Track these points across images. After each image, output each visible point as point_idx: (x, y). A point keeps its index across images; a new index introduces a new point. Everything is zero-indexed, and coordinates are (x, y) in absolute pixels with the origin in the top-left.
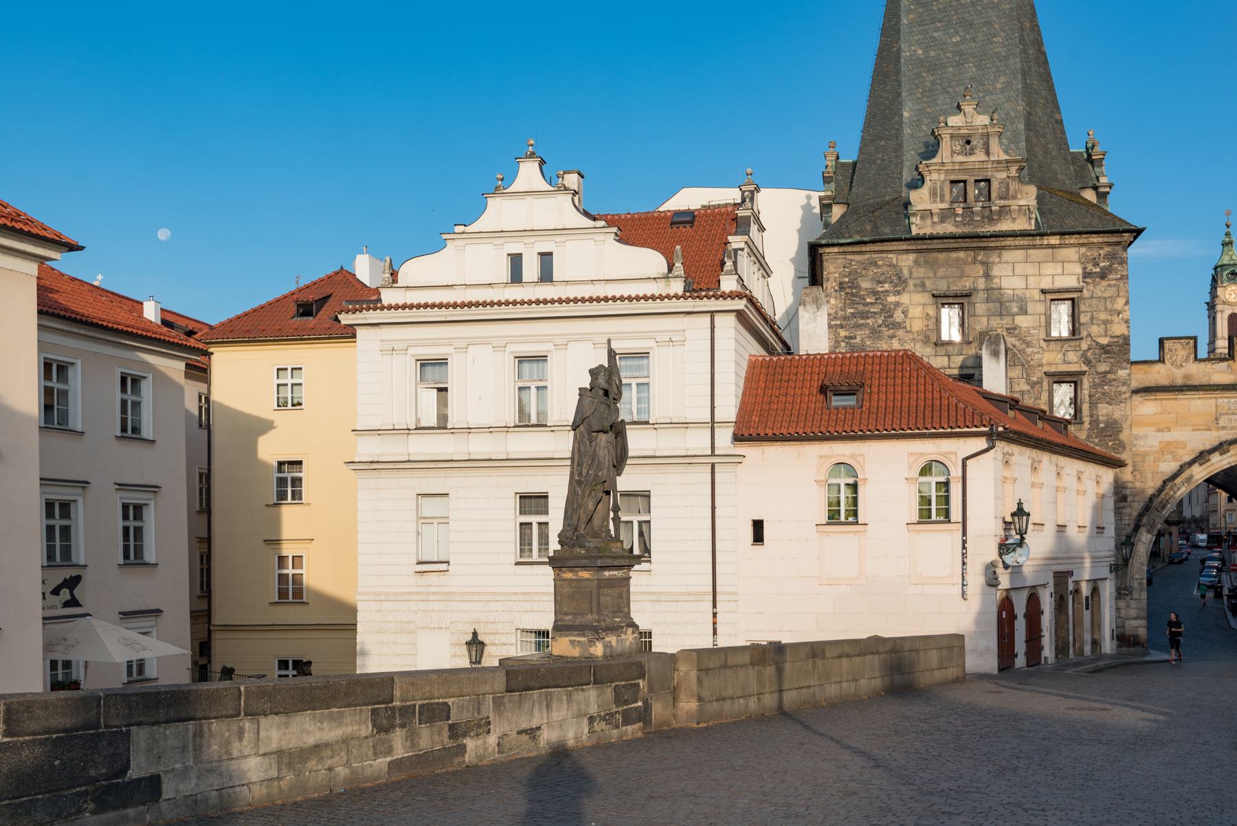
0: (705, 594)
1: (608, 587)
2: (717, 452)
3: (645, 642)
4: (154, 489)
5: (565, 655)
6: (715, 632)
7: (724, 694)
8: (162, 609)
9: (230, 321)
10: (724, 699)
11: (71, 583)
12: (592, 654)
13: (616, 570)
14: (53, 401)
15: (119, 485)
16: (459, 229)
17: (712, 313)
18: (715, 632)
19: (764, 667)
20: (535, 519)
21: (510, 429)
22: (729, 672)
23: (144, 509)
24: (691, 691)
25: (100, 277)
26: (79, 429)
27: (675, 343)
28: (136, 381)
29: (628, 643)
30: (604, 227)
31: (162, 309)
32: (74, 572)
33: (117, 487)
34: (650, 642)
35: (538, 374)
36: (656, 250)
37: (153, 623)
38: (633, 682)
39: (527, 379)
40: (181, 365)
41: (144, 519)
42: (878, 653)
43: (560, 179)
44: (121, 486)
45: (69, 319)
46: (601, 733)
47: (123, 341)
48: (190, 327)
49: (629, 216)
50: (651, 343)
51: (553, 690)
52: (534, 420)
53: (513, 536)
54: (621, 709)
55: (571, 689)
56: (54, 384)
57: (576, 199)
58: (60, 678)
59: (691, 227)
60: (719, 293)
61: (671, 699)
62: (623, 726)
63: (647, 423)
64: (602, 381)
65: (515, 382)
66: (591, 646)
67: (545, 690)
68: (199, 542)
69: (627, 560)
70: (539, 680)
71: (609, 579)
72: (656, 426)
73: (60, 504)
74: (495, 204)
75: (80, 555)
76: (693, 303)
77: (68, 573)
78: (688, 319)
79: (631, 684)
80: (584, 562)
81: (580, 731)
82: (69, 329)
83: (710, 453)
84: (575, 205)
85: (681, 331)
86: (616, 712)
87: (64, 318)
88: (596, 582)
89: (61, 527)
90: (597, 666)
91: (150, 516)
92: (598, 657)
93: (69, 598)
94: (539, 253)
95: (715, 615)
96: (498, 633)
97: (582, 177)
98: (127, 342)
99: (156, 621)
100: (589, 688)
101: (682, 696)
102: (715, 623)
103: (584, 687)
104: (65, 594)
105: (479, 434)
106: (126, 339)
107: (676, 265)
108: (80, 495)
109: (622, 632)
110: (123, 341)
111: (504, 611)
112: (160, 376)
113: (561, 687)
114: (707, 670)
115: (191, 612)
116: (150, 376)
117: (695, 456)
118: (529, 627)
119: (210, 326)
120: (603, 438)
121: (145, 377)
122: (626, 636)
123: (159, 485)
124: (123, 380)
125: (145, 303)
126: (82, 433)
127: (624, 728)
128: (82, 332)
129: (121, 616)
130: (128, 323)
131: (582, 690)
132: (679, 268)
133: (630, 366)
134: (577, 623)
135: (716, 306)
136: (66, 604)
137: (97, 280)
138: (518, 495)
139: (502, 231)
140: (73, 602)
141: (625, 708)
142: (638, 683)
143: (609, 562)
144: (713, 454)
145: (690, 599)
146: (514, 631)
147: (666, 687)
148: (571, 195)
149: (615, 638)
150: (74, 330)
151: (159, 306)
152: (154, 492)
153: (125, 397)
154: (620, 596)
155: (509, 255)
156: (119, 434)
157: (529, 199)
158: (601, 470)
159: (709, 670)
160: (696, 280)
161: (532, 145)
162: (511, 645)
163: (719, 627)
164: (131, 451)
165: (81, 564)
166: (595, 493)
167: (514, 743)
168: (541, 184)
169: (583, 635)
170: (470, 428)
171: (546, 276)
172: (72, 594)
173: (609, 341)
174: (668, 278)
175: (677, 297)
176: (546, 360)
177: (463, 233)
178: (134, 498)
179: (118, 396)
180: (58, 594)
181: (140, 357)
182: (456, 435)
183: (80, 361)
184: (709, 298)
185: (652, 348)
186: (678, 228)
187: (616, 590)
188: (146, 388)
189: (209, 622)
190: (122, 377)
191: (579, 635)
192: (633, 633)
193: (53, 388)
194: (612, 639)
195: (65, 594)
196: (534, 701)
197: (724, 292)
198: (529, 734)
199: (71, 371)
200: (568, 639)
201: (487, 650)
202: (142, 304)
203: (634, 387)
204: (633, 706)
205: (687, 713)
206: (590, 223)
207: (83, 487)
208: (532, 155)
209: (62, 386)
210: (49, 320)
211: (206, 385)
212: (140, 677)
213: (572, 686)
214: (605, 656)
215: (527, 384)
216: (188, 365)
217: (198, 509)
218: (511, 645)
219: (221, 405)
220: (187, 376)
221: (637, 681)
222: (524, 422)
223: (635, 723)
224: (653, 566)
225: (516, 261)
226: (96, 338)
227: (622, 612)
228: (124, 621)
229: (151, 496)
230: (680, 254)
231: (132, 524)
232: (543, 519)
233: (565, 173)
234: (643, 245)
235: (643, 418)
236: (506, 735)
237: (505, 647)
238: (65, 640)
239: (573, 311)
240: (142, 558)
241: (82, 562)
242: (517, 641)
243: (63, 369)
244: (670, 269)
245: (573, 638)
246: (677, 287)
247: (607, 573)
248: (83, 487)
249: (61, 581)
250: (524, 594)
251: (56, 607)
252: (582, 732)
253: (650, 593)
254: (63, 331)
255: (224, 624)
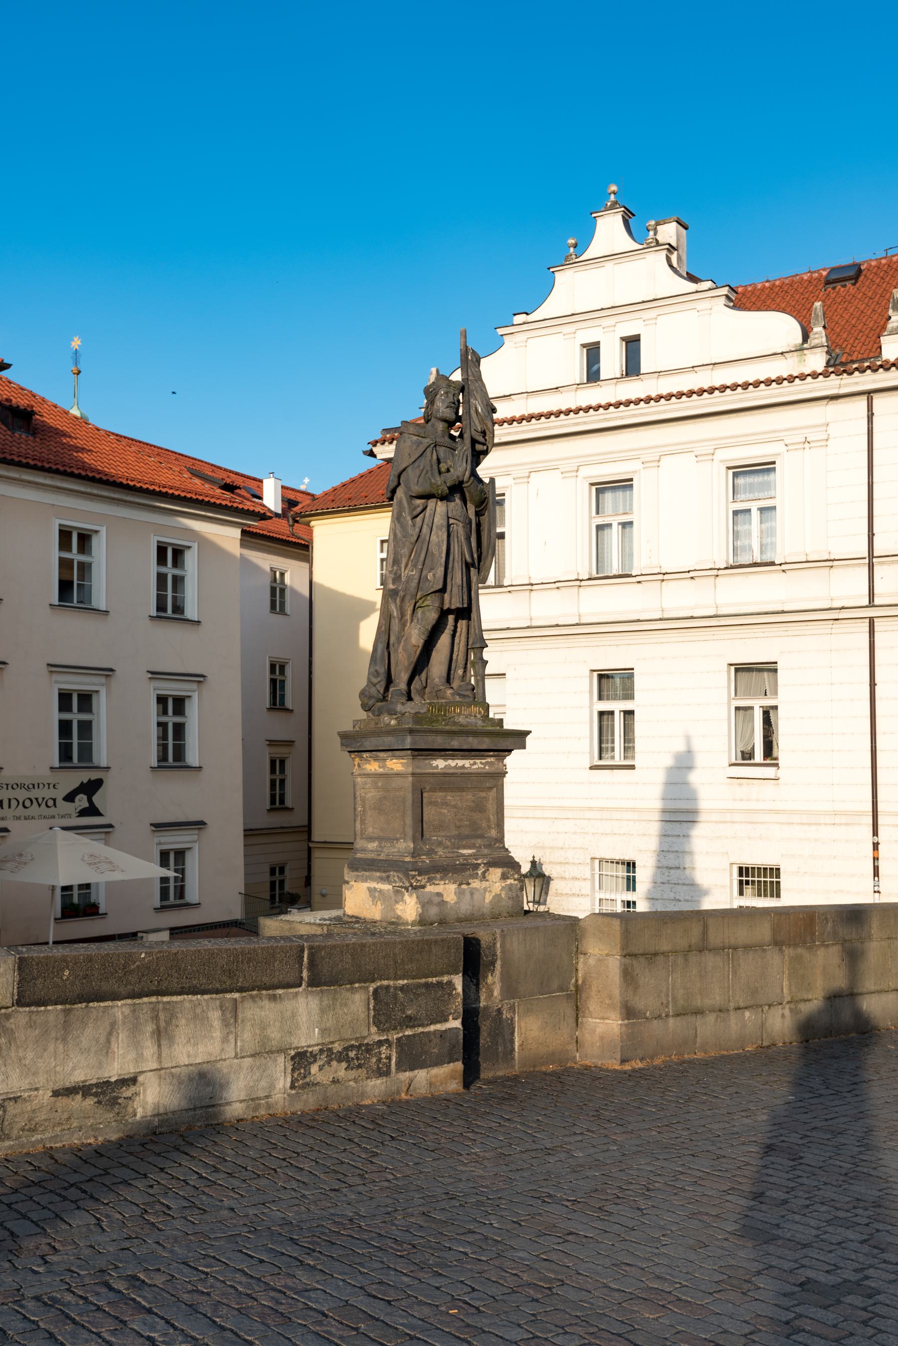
0: (860, 814)
1: (441, 789)
2: (877, 601)
3: (772, 882)
4: (199, 678)
5: (362, 916)
6: (876, 872)
7: (698, 1002)
8: (114, 825)
9: (335, 489)
10: (699, 1012)
11: (91, 787)
12: (399, 917)
13: (464, 758)
14: (73, 574)
15: (152, 673)
16: (518, 319)
17: (869, 394)
18: (876, 872)
19: (810, 948)
20: (617, 706)
21: (583, 583)
22: (710, 960)
23: (187, 702)
24: (610, 997)
25: (306, 480)
26: (103, 607)
27: (812, 445)
28: (178, 553)
29: (488, 898)
30: (710, 289)
31: (283, 487)
32: (94, 775)
33: (150, 676)
34: (778, 883)
35: (625, 506)
36: (795, 318)
37: (195, 838)
38: (434, 980)
39: (610, 513)
40: (236, 533)
41: (186, 715)
42: (125, 1098)
43: (651, 233)
44: (155, 675)
45: (93, 480)
46: (332, 1089)
47: (158, 504)
48: (228, 481)
49: (767, 285)
50: (778, 448)
51: (175, 998)
52: (615, 570)
53: (588, 730)
54: (394, 1036)
55: (236, 995)
56: (74, 555)
57: (674, 258)
58: (75, 900)
59: (854, 284)
60: (879, 363)
61: (570, 1012)
62: (400, 1067)
63: (772, 564)
64: (442, 407)
65: (591, 518)
66: (397, 902)
67: (153, 999)
68: (269, 745)
69: (486, 740)
70: (133, 978)
71: (445, 775)
72: (784, 567)
73: (79, 695)
74: (564, 279)
75: (102, 755)
76: (838, 382)
77: (85, 776)
78: (833, 406)
79: (427, 986)
80: (389, 741)
81: (263, 1083)
82: (89, 490)
83: (866, 602)
84: (671, 266)
85: (822, 425)
86: (380, 1043)
87: (79, 477)
88: (410, 779)
89: (79, 721)
90: (320, 949)
91: (193, 710)
92: (407, 924)
93: (87, 805)
94: (623, 339)
95: (876, 846)
96: (567, 863)
97: (686, 228)
98: (163, 505)
99: (198, 835)
100: (297, 994)
101: (593, 1005)
102: (876, 859)
103: (280, 991)
104: (82, 801)
105: (544, 592)
106: (161, 502)
107: (815, 330)
108: (103, 685)
109: (475, 876)
110: (158, 504)
111: (575, 833)
112: (206, 544)
113: (203, 992)
114: (651, 956)
115: (245, 830)
116: (195, 546)
117: (843, 608)
118: (618, 857)
119: (313, 495)
120: (439, 509)
121: (189, 547)
122: (485, 884)
123: (205, 674)
124: (162, 550)
125: (265, 481)
126: (106, 612)
127: (406, 1076)
128: (95, 491)
129: (153, 828)
130: (177, 484)
131: (273, 998)
132: (819, 333)
133: (750, 484)
134: (382, 857)
135: (874, 381)
136: (83, 813)
137: (304, 483)
138: (595, 674)
139: (573, 315)
140: (92, 811)
141: (408, 1032)
142: (450, 983)
143: (439, 741)
144: (871, 604)
145: (837, 821)
146: (589, 861)
147: (555, 985)
148: (665, 252)
149: (453, 887)
150: (95, 491)
151: (280, 483)
152: (199, 682)
153: (163, 570)
154: (479, 807)
155: (583, 346)
156: (154, 613)
157: (609, 265)
158: (432, 569)
159: (656, 954)
160: (847, 350)
161: (614, 193)
162: (585, 880)
163: (881, 864)
164: (171, 633)
165: (102, 765)
166: (423, 613)
167: (41, 1116)
168: (626, 243)
169: (387, 879)
170: (532, 585)
171: (632, 367)
172: (90, 801)
173: (464, 334)
174: (802, 350)
175: (815, 375)
176: (631, 486)
177: (524, 323)
178: (172, 689)
179: (153, 569)
180: (73, 801)
181: (179, 522)
182: (515, 594)
183: (104, 528)
184: (862, 371)
185: (779, 454)
186: (834, 288)
187: (469, 796)
188: (191, 559)
189: (309, 839)
190: (159, 547)
191: (382, 880)
192: (504, 877)
193: (72, 561)
194: (448, 890)
195: (82, 801)
196: (113, 1025)
197: (887, 361)
198: (96, 1095)
199: (94, 540)
200: (366, 885)
201: (553, 885)
202: (261, 481)
203: (755, 514)
204: (432, 1028)
205: (602, 1038)
206: (691, 287)
207: (107, 676)
208: (614, 205)
209: (83, 558)
210: (45, 478)
211: (306, 565)
212: (179, 902)
213: (241, 990)
214: (422, 921)
215: (606, 521)
216: (244, 532)
217: (268, 706)
218: (585, 880)
219: (322, 586)
220: (243, 544)
221: (445, 979)
222: (601, 576)
223: (437, 1063)
224: (780, 773)
225: (593, 352)
226: (125, 501)
227: (482, 837)
228: (157, 834)
229: (194, 686)
230: (820, 314)
231: (75, 717)
232: (627, 705)
233: (658, 224)
234: (768, 309)
235: (767, 558)
236: (16, 1099)
237: (577, 883)
238: (21, 855)
239: (665, 412)
240: (90, 759)
241: (104, 764)
242: (593, 875)
243: (85, 539)
244: (806, 337)
245: (373, 885)
246: (817, 360)
247: (440, 764)
248: (107, 676)
249: (77, 785)
250: (602, 809)
251: (70, 816)
252: (272, 1086)
253: (777, 812)
254: (83, 493)
255: (323, 840)
